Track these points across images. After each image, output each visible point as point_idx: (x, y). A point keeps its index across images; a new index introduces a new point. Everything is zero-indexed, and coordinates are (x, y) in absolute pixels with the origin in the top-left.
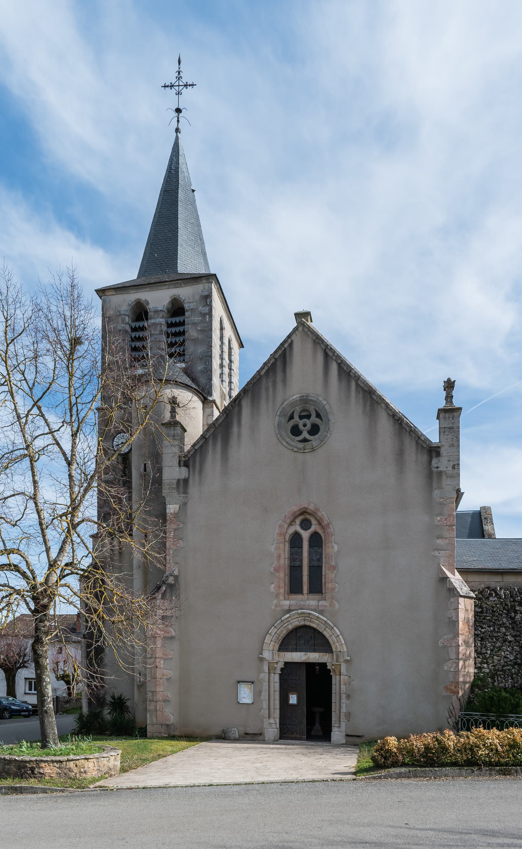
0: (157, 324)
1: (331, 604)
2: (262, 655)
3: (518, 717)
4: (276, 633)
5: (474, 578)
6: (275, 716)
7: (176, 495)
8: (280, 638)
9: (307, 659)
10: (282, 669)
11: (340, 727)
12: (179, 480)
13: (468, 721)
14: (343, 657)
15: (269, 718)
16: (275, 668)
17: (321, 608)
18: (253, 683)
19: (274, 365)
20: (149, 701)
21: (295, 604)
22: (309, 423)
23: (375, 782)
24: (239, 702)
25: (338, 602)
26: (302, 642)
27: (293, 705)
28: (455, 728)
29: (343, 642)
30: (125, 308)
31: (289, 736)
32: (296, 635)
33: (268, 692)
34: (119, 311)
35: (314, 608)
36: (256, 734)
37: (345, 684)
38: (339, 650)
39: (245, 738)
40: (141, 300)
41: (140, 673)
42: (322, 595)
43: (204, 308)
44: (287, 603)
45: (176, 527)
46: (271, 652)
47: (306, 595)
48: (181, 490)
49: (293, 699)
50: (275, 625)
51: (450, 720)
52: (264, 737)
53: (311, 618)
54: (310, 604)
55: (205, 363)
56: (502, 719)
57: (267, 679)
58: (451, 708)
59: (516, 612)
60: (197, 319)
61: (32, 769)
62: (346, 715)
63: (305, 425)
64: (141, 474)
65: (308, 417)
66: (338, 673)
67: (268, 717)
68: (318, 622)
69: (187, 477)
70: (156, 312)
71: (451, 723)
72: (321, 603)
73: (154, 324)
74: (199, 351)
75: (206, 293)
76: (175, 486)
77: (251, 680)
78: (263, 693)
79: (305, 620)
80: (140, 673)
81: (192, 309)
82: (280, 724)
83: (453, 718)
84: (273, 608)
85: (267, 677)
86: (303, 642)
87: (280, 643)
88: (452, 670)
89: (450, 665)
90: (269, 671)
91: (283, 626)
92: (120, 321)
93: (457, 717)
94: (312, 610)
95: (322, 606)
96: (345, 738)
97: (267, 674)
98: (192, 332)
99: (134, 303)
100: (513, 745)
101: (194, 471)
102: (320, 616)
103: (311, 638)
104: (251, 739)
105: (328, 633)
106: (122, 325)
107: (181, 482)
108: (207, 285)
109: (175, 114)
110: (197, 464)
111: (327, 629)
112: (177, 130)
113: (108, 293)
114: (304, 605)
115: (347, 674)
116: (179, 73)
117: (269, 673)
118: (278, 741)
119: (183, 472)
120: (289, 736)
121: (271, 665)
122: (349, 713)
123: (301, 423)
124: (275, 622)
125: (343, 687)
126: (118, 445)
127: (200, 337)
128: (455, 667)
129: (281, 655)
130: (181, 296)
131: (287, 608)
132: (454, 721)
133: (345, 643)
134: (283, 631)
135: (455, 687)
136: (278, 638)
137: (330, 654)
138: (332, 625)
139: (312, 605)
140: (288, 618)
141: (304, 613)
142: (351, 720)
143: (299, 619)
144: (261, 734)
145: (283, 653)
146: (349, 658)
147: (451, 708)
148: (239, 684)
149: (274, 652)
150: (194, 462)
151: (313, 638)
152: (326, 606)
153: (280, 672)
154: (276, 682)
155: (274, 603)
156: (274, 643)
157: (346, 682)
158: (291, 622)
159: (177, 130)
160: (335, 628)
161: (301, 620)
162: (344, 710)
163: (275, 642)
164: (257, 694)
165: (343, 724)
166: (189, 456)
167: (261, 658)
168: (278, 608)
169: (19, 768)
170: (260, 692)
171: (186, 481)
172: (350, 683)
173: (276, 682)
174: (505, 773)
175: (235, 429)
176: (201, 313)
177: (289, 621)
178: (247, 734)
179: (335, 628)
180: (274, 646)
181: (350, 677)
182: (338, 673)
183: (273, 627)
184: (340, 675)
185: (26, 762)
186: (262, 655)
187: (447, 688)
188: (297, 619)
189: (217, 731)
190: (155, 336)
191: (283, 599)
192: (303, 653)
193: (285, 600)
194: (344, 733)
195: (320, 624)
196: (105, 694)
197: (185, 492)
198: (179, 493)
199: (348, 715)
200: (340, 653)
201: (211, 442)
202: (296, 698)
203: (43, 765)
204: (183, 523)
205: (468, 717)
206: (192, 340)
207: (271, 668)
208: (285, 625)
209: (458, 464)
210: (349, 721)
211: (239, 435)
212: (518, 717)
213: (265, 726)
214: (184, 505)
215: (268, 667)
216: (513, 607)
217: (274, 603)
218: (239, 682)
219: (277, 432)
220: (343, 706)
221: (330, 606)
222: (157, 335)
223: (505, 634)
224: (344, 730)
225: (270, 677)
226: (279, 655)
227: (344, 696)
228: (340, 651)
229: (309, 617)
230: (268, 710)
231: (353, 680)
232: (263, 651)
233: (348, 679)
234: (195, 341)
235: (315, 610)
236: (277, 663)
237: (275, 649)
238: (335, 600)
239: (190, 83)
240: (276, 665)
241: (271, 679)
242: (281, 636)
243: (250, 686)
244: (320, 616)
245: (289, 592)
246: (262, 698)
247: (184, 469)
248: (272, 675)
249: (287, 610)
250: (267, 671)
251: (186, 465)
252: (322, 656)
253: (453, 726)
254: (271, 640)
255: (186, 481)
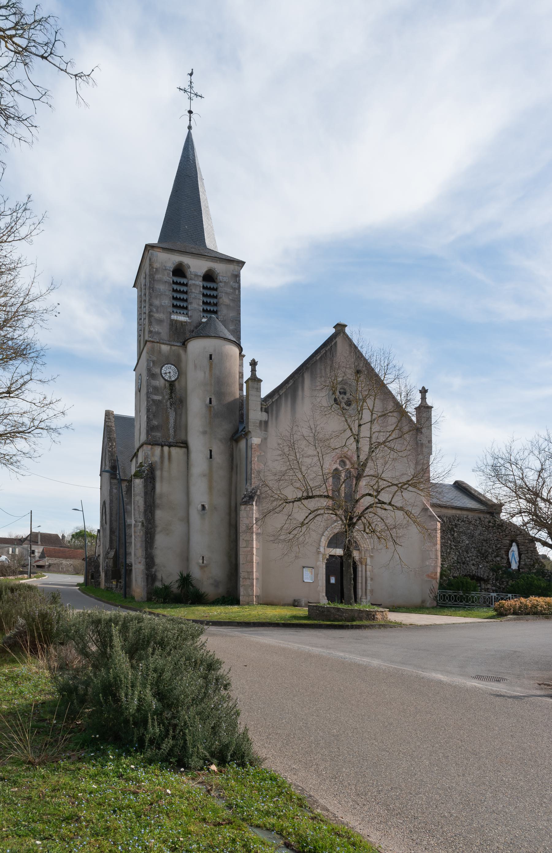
0: (197, 285)
3: (476, 593)
5: (438, 510)
7: (259, 431)
12: (261, 421)
13: (444, 595)
20: (243, 579)
22: (346, 397)
23: (508, 622)
24: (304, 581)
27: (333, 584)
28: (435, 600)
30: (171, 266)
34: (165, 267)
40: (183, 262)
41: (203, 557)
43: (234, 284)
45: (259, 454)
48: (263, 428)
49: (333, 580)
51: (431, 595)
55: (236, 325)
56: (467, 595)
58: (432, 588)
59: (454, 531)
60: (229, 290)
61: (374, 616)
62: (370, 591)
63: (343, 398)
64: (206, 405)
65: (345, 393)
69: (267, 420)
70: (196, 275)
71: (432, 597)
73: (194, 284)
74: (231, 315)
75: (236, 273)
76: (258, 425)
80: (203, 557)
81: (225, 282)
83: (433, 594)
88: (432, 565)
89: (431, 562)
92: (166, 274)
93: (436, 593)
98: (225, 299)
99: (177, 263)
100: (548, 604)
101: (272, 416)
106: (168, 278)
107: (263, 423)
108: (236, 267)
109: (188, 114)
110: (274, 412)
112: (190, 128)
113: (155, 249)
116: (191, 83)
119: (264, 416)
122: (372, 590)
123: (346, 397)
125: (368, 573)
126: (166, 373)
127: (231, 304)
128: (435, 563)
130: (216, 269)
132: (434, 595)
135: (435, 575)
147: (432, 588)
150: (272, 411)
159: (190, 128)
162: (369, 588)
164: (316, 576)
165: (369, 597)
166: (268, 405)
169: (368, 615)
171: (266, 423)
174: (547, 618)
175: (300, 393)
176: (232, 287)
185: (371, 611)
187: (428, 576)
189: (290, 600)
190: (196, 295)
196: (155, 572)
197: (266, 430)
198: (261, 430)
199: (372, 591)
201: (283, 399)
203: (377, 613)
204: (264, 452)
205: (444, 593)
206: (225, 305)
209: (431, 441)
210: (372, 595)
211: (303, 398)
212: (476, 593)
213: (320, 598)
214: (265, 440)
216: (452, 528)
218: (304, 567)
219: (328, 401)
220: (369, 585)
222: (196, 293)
223: (450, 544)
227: (369, 579)
234: (228, 306)
239: (199, 94)
247: (264, 414)
251: (266, 411)
253: (434, 599)
255: (266, 423)
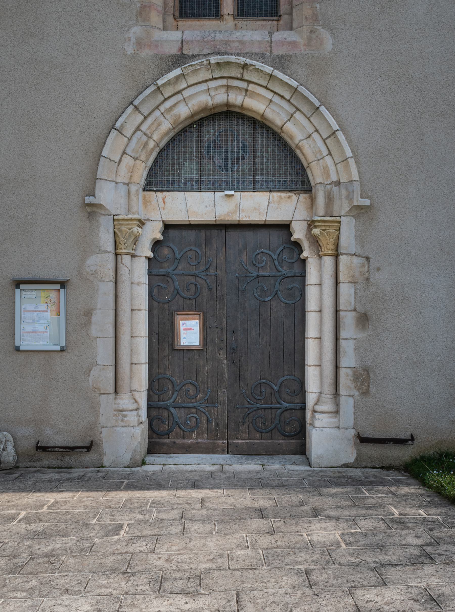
1: (310, 39)
2: (94, 196)
4: (138, 129)
6: (134, 387)
8: (151, 144)
9: (233, 212)
10: (156, 245)
11: (337, 412)
14: (349, 198)
15: (116, 392)
16: (136, 240)
17: (279, 51)
18: (63, 284)
19: (191, 126)
21: (199, 38)
24: (17, 349)
25: (332, 31)
26: (219, 161)
27: (189, 350)
29: (349, 153)
31: (178, 441)
32: (200, 141)
33: (112, 313)
35: (257, 51)
36: (73, 448)
37: (354, 282)
38: (334, 178)
39: (39, 460)
42: (278, 20)
44: (175, 35)
46: (123, 190)
47: (230, 18)
50: (136, 103)
52: (101, 455)
53: (249, 82)
54: (246, 39)
57: (111, 272)
62: (356, 377)
66: (328, 248)
67: (112, 390)
68: (269, 95)
72: (277, 36)
77: (60, 277)
78: (97, 317)
79: (228, 87)
82: (150, 407)
84: (130, 49)
85: (111, 265)
86: (221, 163)
87: (150, 163)
90: (116, 249)
91: (162, 108)
94: (252, 56)
95: (282, 43)
96: (355, 445)
97: (111, 257)
102: (277, 73)
103: (244, 148)
104: (59, 463)
105: (302, 128)
111: (298, 115)
114: (227, 43)
115: (359, 252)
117: (116, 255)
118: (144, 463)
120: (178, 441)
121: (123, 228)
122: (367, 370)
124: (134, 94)
129: (154, 202)
131: (174, 51)
133: (355, 156)
134: (159, 125)
136: (146, 144)
137: (303, 196)
138: (317, 103)
139: (252, 42)
140: (177, 78)
141: (228, 63)
142: (373, 390)
143: (212, 84)
144: (89, 448)
145: (159, 194)
146: (367, 202)
148: (18, 291)
149: (134, 188)
151: (250, 152)
152: (293, 44)
153: (151, 255)
154: (138, 284)
155: (131, 35)
156: (132, 162)
157: (357, 274)
158: (186, 93)
160: (322, 109)
161: (216, 88)
163: (135, 159)
167: (91, 205)
168: (146, 52)
170: (88, 314)
172: (368, 279)
173: (138, 284)
177: (180, 92)
178: (44, 449)
179: (322, 109)
180: (132, 170)
181: (368, 258)
182: (328, 248)
183: (131, 108)
184: (336, 256)
186: (94, 196)
188: (203, 87)
191: (161, 26)
192: (219, 194)
193: (165, 28)
194: (352, 432)
195: (276, 99)
200: (336, 189)
202: (196, 329)
207: (122, 239)
208: (168, 104)
210: (366, 393)
213: (102, 420)
215: (112, 235)
217: (131, 35)
218: (18, 284)
221: (308, 44)
224: (351, 423)
225: (120, 265)
226: (146, 202)
228: (338, 183)
229: (242, 79)
230: (112, 368)
231: (378, 269)
232: (98, 184)
233: (363, 266)
235: (261, 57)
236: (141, 223)
237: (135, 179)
238: (324, 27)
240: (136, 230)
241: (124, 271)
242: (156, 137)
243: (53, 295)
244: (277, 73)
245: (177, 13)
246: (94, 331)
248: (126, 259)
249: (172, 57)
250: (110, 247)
252: (279, 202)
254: (124, 153)
